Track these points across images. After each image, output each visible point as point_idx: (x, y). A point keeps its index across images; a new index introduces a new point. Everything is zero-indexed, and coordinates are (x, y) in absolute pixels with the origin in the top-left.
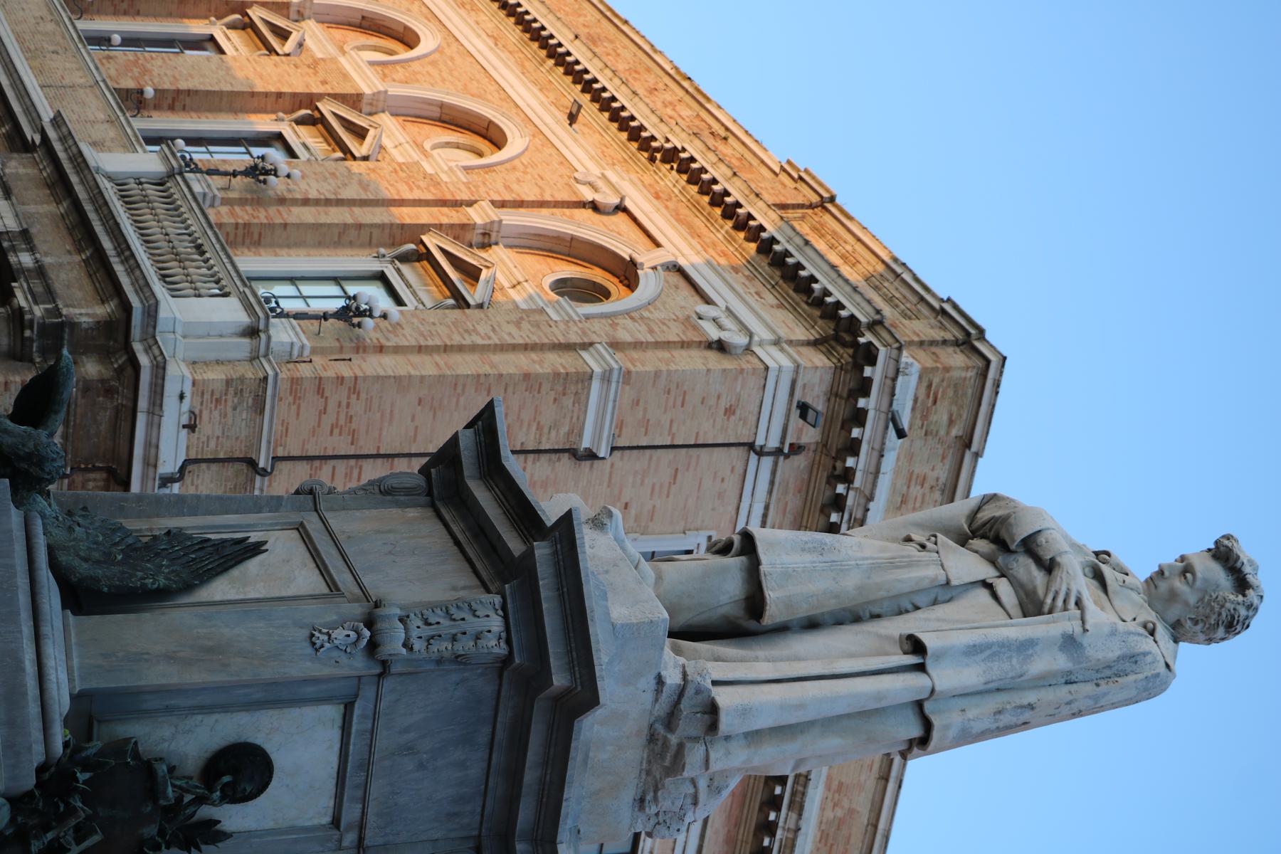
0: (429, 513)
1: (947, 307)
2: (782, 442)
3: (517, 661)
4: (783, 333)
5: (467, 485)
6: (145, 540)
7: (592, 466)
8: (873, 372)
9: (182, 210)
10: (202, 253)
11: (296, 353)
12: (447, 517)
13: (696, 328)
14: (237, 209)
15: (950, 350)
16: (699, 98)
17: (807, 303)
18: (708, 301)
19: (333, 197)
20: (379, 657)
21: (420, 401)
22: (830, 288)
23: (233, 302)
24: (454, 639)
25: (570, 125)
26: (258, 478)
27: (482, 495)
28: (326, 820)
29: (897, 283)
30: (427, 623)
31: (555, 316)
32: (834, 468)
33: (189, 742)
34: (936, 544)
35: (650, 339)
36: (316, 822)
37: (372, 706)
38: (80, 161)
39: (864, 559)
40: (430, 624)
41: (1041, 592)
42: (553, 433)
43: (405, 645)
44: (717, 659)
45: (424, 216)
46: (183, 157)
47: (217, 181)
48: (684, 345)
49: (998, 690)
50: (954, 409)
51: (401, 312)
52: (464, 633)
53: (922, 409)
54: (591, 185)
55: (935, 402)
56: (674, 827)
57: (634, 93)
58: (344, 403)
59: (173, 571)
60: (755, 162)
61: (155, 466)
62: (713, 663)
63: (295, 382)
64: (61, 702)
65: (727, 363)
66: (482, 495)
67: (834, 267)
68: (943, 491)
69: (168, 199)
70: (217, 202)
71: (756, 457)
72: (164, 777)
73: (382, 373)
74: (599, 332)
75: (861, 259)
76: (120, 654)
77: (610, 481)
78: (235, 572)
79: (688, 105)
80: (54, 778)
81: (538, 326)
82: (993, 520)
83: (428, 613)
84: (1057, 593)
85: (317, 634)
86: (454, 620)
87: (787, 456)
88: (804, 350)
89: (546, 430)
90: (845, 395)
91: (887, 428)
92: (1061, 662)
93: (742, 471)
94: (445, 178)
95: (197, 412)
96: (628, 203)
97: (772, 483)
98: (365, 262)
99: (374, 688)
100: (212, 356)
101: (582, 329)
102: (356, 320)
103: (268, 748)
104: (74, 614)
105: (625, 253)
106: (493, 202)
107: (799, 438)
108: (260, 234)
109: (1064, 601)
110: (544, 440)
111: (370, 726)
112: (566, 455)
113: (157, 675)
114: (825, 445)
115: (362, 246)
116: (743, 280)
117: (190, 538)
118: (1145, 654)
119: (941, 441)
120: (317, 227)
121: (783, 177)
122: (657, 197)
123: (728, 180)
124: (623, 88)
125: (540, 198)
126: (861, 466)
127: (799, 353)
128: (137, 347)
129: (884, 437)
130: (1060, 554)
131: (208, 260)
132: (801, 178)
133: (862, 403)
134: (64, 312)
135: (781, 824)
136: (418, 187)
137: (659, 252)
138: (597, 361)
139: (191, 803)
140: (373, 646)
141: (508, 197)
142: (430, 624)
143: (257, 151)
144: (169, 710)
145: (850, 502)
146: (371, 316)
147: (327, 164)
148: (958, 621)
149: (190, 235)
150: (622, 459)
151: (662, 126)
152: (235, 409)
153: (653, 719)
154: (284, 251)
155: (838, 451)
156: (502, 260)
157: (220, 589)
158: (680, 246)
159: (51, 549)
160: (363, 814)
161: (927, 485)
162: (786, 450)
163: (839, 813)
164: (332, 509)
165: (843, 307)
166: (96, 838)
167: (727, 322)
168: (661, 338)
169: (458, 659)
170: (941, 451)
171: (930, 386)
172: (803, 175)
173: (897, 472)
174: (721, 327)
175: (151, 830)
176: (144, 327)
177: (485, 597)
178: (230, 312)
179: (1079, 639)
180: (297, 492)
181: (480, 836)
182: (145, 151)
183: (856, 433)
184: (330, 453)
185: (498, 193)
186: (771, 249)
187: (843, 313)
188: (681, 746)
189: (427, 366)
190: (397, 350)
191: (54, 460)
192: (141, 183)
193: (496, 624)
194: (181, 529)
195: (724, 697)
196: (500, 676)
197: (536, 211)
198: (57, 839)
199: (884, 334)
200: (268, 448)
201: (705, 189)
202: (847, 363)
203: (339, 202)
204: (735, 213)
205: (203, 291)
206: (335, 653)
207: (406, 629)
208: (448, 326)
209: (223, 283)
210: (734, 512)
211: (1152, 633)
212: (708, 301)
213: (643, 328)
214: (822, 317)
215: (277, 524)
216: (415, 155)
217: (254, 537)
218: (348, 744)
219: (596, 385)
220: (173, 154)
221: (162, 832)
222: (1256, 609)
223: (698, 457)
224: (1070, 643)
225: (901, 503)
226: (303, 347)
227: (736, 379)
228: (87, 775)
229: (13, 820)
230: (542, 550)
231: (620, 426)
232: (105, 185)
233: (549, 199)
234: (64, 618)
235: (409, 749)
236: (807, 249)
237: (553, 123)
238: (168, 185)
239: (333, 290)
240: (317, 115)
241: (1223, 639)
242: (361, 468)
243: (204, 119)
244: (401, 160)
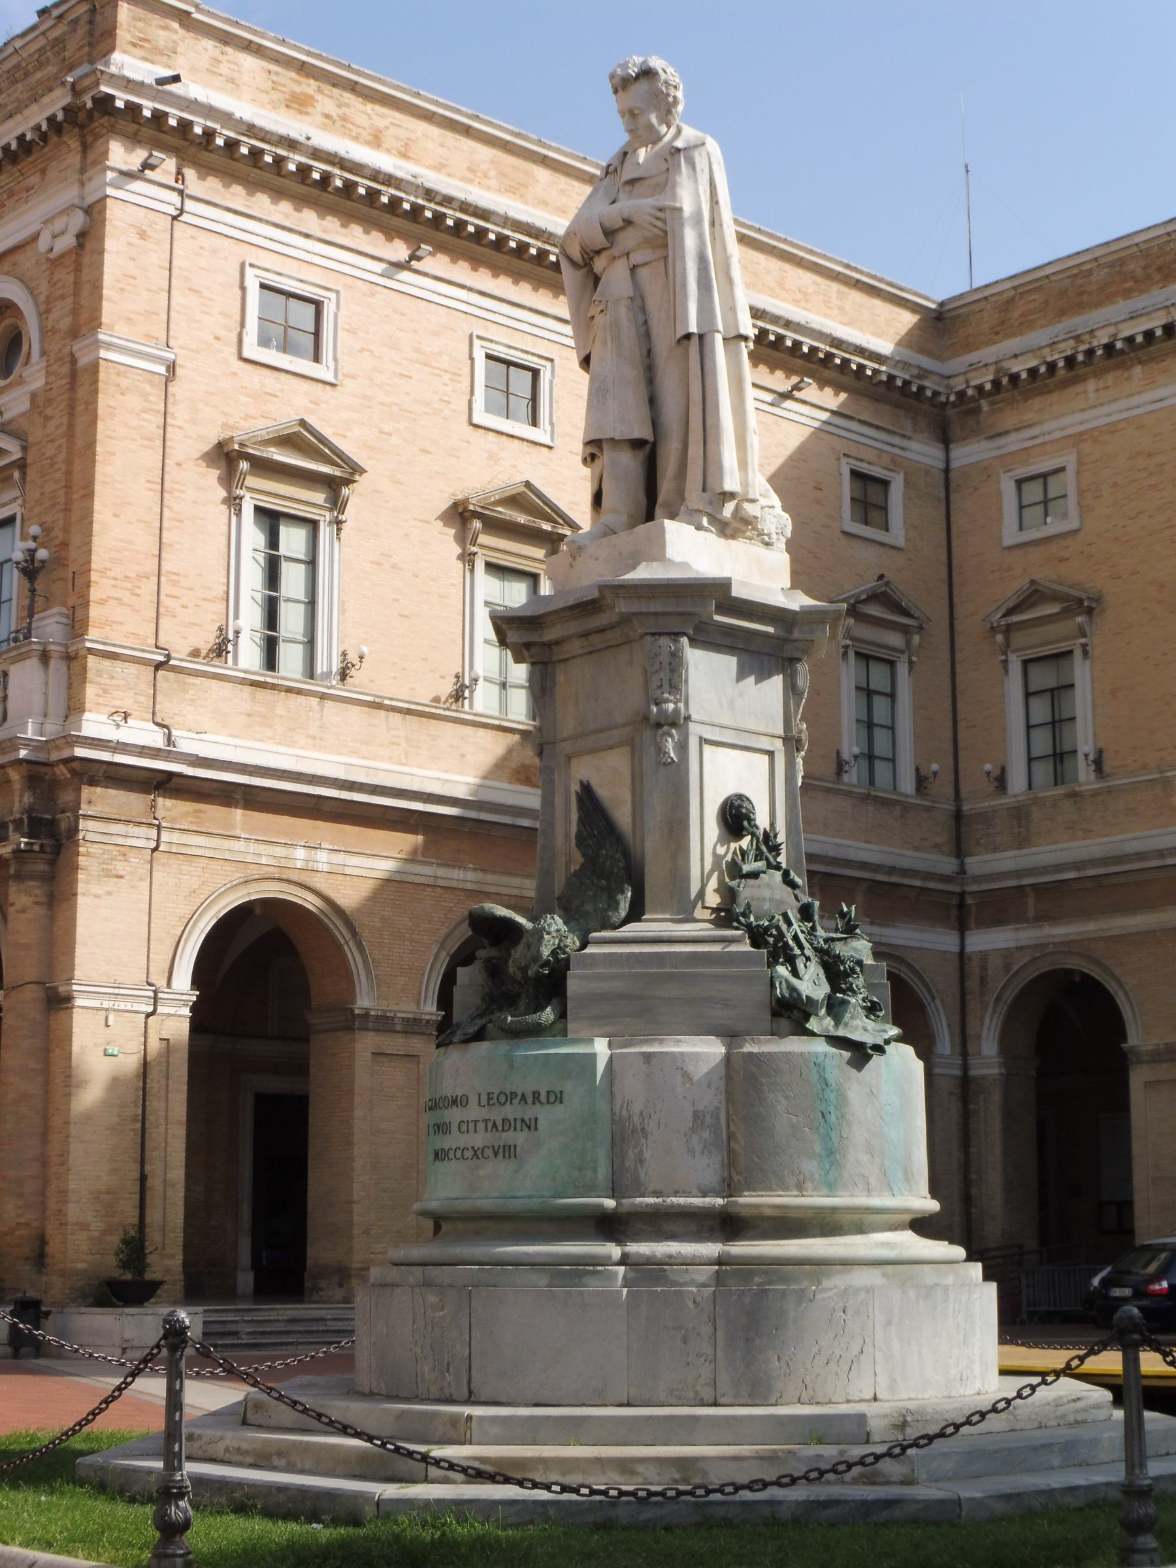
2: (173, 189)
7: (181, 366)
8: (120, 99)
11: (68, 622)
17: (43, 147)
21: (115, 515)
26: (172, 662)
35: (70, 300)
42: (151, 398)
55: (148, 41)
58: (113, 582)
71: (185, 215)
77: (194, 351)
89: (148, 405)
90: (136, 126)
97: (208, 203)
100: (63, 694)
101: (56, 361)
107: (171, 174)
110: (156, 407)
112: (170, 388)
135: (499, 229)
146: (35, 551)
150: (176, 338)
157: (623, 816)
161: (220, 57)
163: (493, 173)
167: (59, 224)
171: (134, 45)
200: (148, 652)
212: (35, 237)
213: (59, 304)
217: (575, 787)
223: (180, 268)
231: (148, 336)
235: (732, 702)
242: (168, 572)
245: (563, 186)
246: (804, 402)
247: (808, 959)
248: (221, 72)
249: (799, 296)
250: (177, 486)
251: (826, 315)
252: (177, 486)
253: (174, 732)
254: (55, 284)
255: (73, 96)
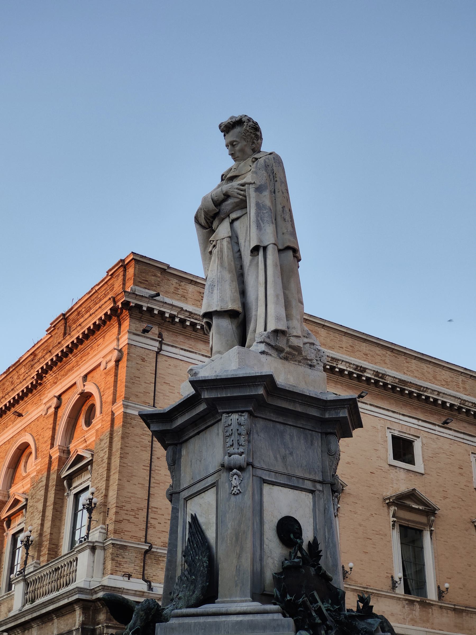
0: (184, 445)
1: (110, 273)
2: (157, 341)
3: (251, 409)
4: (115, 337)
5: (173, 429)
6: (186, 566)
9: (40, 576)
10: (59, 568)
11: (104, 531)
12: (187, 437)
13: (109, 371)
14: (42, 553)
15: (127, 273)
16: (17, 365)
17: (104, 327)
18: (99, 365)
19: (41, 513)
20: (245, 466)
21: (128, 481)
22: (99, 317)
23: (80, 556)
24: (240, 434)
25: (23, 416)
26: (153, 550)
27: (180, 421)
28: (310, 495)
29: (99, 292)
30: (232, 445)
31: (100, 426)
32: (169, 322)
33: (275, 552)
34: (213, 241)
36: (311, 501)
37: (265, 472)
38: (15, 618)
39: (218, 269)
40: (233, 444)
41: (237, 200)
43: (241, 455)
44: (255, 331)
45: (54, 476)
46: (18, 575)
47: (30, 561)
48: (116, 375)
49: (275, 220)
50: (150, 274)
51: (92, 487)
52: (238, 430)
53: (149, 286)
54: (48, 409)
56: (322, 354)
57: (12, 390)
58: (126, 512)
59: (201, 554)
60: (46, 344)
61: (144, 592)
62: (257, 330)
63: (115, 532)
64: (257, 606)
65: (125, 358)
66: (180, 421)
67: (90, 315)
68: (181, 281)
69: (35, 581)
70: (38, 562)
72: (290, 562)
73: (116, 496)
74: (108, 409)
75: (89, 305)
76: (236, 579)
78: (204, 527)
79: (20, 370)
80: (288, 610)
81: (103, 432)
82: (206, 218)
83: (228, 445)
84: (238, 193)
85: (233, 492)
86: (232, 434)
87: (163, 340)
88: (122, 329)
89: (144, 432)
90: (141, 315)
91: (155, 300)
92: (266, 193)
93: (167, 357)
94: (38, 467)
95: (124, 573)
96: (57, 394)
97: (172, 346)
98: (70, 501)
99: (257, 470)
102: (93, 505)
103: (280, 518)
104: (217, 599)
105: (77, 397)
106: (51, 448)
107: (156, 334)
108: (53, 544)
109: (242, 191)
110: (148, 433)
111: (273, 473)
113: (246, 563)
114: (160, 324)
115: (63, 502)
116: (92, 351)
117: (187, 547)
118: (265, 162)
119: (162, 280)
120: (53, 520)
121: (53, 334)
122: (56, 383)
123: (52, 354)
124: (10, 394)
125: (51, 429)
126: (169, 311)
127: (123, 331)
128: (94, 597)
129: (159, 301)
130: (222, 191)
131: (61, 566)
132: (54, 327)
133: (145, 309)
134: (78, 627)
136: (41, 478)
137: (78, 383)
138: (119, 410)
139: (301, 553)
140: (241, 469)
141: (49, 442)
142: (233, 444)
143: (19, 544)
144: (261, 559)
145: (182, 317)
147: (27, 516)
148: (246, 234)
149: (50, 573)
151: (27, 379)
152: (124, 558)
153: (278, 357)
154: (62, 535)
155: (163, 320)
156: (75, 446)
157: (211, 534)
158: (75, 377)
159: (188, 607)
160: (309, 480)
162: (161, 339)
164: (180, 486)
165: (107, 312)
166: (315, 594)
168: (112, 384)
169: (249, 434)
170: (166, 281)
171: (141, 282)
172: (53, 326)
173: (172, 298)
174: (110, 361)
175: (312, 571)
176: (87, 593)
177: (223, 421)
178: (84, 558)
179: (257, 186)
180: (171, 501)
181: (321, 433)
182: (14, 591)
183: (156, 312)
184: (145, 519)
185: (47, 446)
186: (81, 339)
187: (109, 313)
188: (290, 347)
189: (115, 477)
190: (107, 489)
191: (149, 603)
192: (27, 593)
193: (235, 417)
194: (182, 552)
195: (271, 327)
196: (257, 417)
197: (57, 431)
198: (315, 611)
199: (119, 297)
201: (55, 364)
202: (129, 313)
203: (44, 511)
204: (65, 352)
205: (74, 569)
206: (242, 485)
207: (234, 454)
208: (99, 469)
209: (72, 560)
210: (183, 362)
211: (256, 159)
212: (99, 365)
213: (108, 391)
214: (110, 321)
215: (184, 510)
216: (28, 479)
217: (189, 519)
218: (280, 483)
219: (129, 411)
220: (16, 579)
221: (313, 566)
222: (250, 118)
223: (160, 374)
224: (259, 189)
225: (184, 298)
226: (102, 528)
227: (131, 356)
228: (288, 596)
229: (306, 630)
230: (206, 395)
232: (28, 606)
233: (52, 425)
234: (218, 603)
235: (284, 458)
236: (83, 325)
237: (20, 424)
238: (29, 581)
239: (80, 514)
240: (6, 519)
241: (261, 133)
242: (152, 507)
243: (3, 566)
244: (29, 485)
245: (332, 338)
246: (450, 429)
247: (329, 628)
248: (179, 293)
249: (444, 383)
250: (157, 468)
251: (457, 391)
252: (157, 468)
253: (152, 584)
254: (107, 383)
255: (114, 303)
